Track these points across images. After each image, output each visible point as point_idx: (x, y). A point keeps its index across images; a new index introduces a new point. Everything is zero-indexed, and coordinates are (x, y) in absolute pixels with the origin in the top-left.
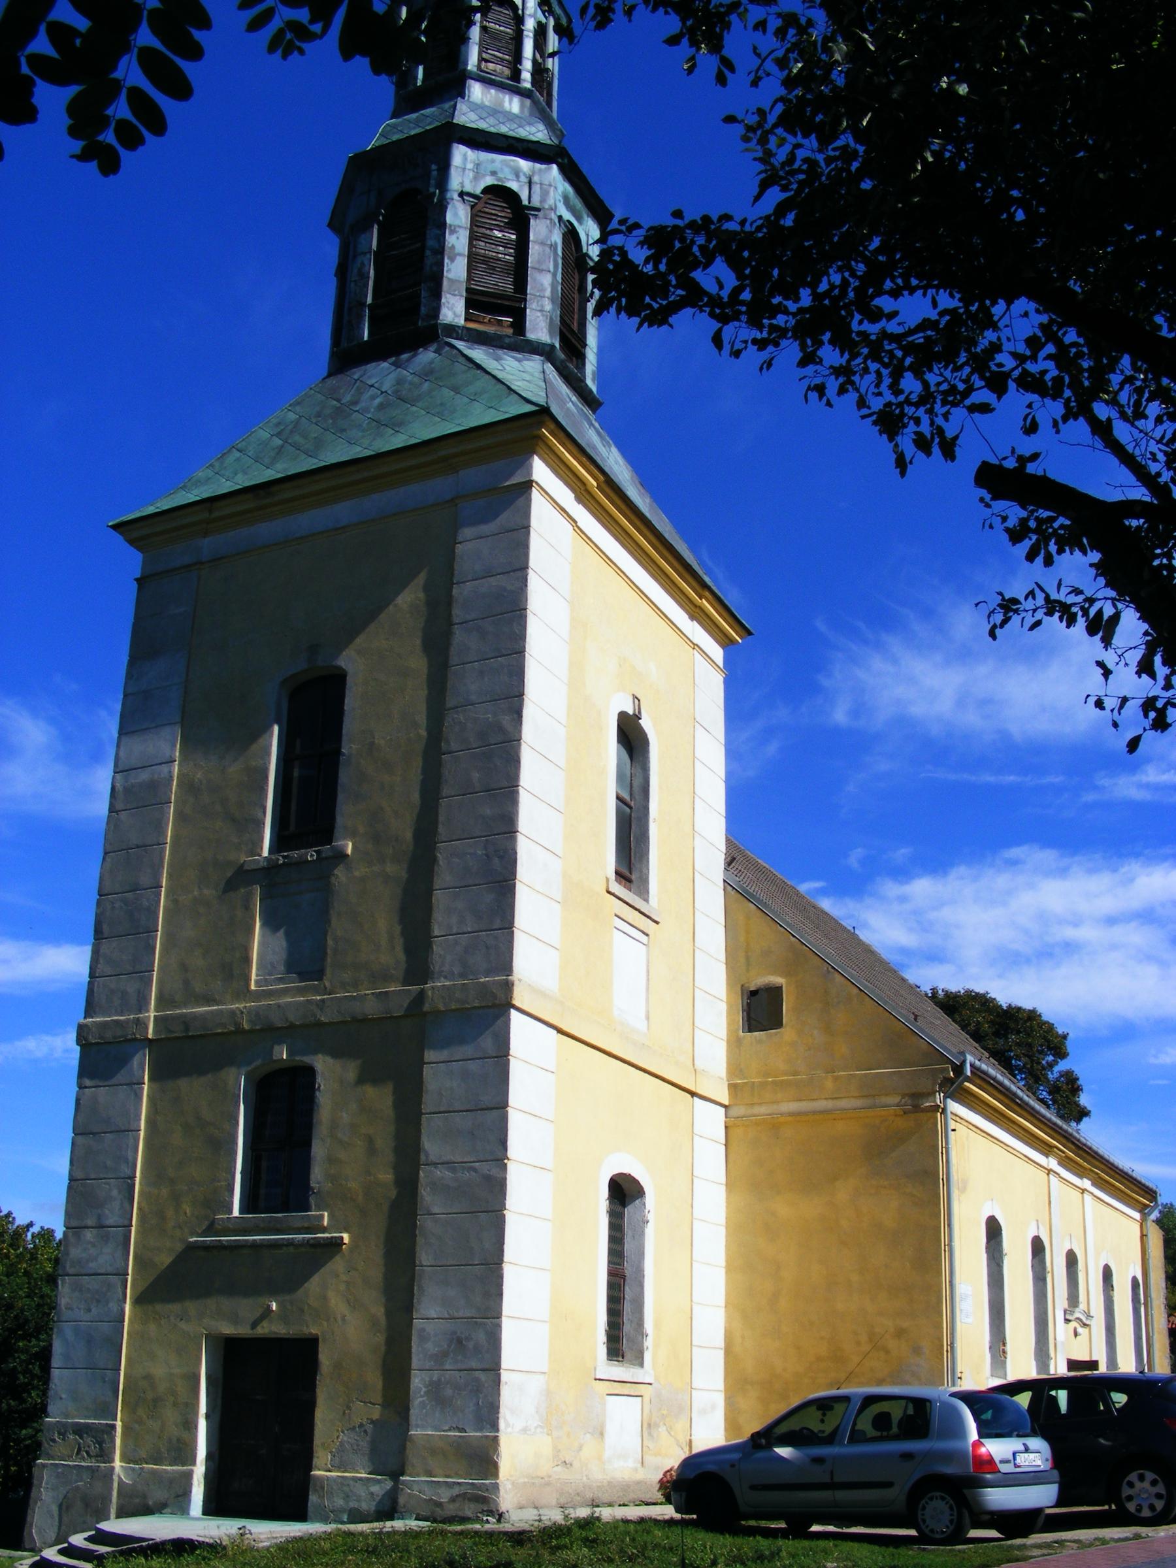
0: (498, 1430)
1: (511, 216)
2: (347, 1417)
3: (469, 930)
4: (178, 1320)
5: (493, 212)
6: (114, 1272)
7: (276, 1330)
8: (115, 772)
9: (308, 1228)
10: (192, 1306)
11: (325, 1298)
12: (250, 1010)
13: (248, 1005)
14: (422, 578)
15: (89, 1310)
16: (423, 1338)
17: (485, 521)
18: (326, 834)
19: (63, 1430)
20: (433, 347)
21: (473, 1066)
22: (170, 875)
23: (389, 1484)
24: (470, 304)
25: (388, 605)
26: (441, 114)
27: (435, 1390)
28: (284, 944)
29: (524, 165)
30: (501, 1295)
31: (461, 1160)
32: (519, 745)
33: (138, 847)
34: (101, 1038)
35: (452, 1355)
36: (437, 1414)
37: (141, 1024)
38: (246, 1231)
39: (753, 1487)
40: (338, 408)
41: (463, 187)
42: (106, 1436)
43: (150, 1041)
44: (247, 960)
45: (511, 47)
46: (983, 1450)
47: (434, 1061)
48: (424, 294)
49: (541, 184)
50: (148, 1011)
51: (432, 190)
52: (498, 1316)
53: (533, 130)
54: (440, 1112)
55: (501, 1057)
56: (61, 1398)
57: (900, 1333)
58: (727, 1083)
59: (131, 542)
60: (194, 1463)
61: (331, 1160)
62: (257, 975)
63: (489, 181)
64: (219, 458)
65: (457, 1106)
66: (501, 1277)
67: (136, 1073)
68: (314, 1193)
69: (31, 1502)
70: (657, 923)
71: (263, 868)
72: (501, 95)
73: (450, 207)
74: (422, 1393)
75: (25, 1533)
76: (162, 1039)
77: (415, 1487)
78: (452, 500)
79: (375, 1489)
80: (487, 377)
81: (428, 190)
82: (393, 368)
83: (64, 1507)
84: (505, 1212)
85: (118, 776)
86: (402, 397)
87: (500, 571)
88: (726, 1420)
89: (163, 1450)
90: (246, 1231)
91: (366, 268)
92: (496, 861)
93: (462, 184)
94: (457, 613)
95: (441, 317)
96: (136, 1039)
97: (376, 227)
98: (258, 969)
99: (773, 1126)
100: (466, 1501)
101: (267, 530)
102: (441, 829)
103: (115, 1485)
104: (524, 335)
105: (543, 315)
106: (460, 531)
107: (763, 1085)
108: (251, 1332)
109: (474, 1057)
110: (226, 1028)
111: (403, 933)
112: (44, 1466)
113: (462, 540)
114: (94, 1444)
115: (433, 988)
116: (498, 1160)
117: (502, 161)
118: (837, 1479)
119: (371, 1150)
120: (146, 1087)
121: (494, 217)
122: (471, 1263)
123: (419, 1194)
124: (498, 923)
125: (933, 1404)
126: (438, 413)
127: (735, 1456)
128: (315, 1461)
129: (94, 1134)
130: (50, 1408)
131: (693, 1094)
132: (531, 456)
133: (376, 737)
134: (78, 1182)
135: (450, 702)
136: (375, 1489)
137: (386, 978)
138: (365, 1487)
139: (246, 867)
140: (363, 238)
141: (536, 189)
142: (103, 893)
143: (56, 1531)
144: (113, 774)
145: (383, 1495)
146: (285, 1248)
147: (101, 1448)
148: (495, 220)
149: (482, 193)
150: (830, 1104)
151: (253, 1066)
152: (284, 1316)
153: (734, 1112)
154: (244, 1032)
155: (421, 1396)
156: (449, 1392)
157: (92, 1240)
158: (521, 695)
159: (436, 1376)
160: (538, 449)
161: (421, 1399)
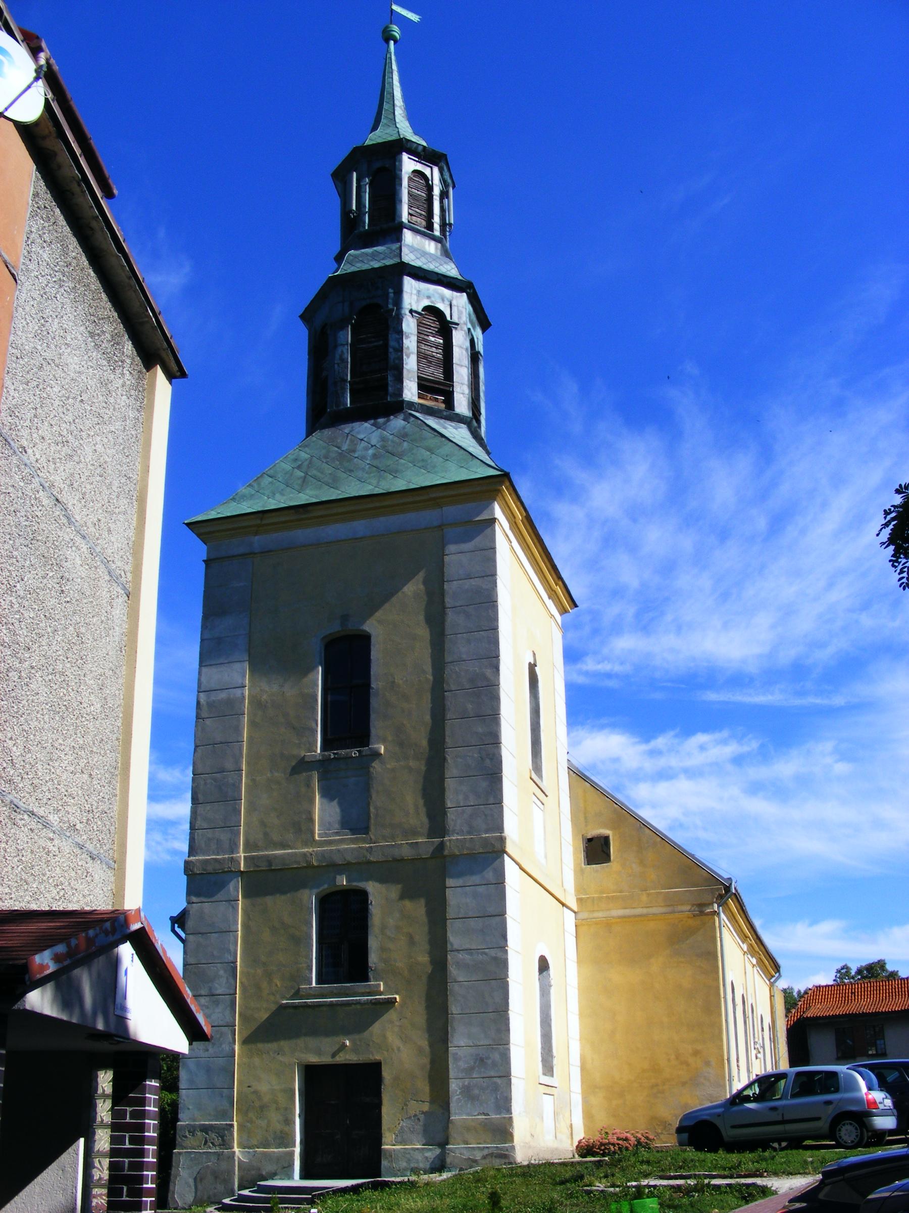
0: (511, 1114)
1: (438, 326)
2: (405, 1111)
3: (472, 804)
4: (276, 1054)
5: (428, 323)
6: (225, 1024)
7: (350, 1058)
8: (199, 692)
9: (369, 993)
10: (284, 1044)
11: (384, 1036)
12: (317, 853)
13: (315, 849)
14: (421, 575)
15: (207, 1050)
16: (457, 1059)
17: (464, 541)
18: (362, 737)
19: (192, 1130)
20: (402, 416)
21: (481, 889)
22: (248, 763)
23: (438, 1151)
24: (421, 387)
25: (397, 592)
26: (390, 253)
27: (467, 1091)
28: (338, 810)
29: (447, 293)
30: (508, 1030)
31: (475, 948)
32: (499, 689)
33: (221, 743)
34: (205, 870)
35: (477, 1069)
36: (469, 1105)
37: (236, 861)
38: (323, 996)
39: (733, 1127)
40: (340, 454)
41: (411, 306)
42: (226, 1132)
43: (242, 872)
44: (311, 820)
45: (425, 206)
46: (870, 1097)
47: (453, 886)
48: (390, 378)
49: (458, 306)
50: (239, 853)
51: (390, 306)
52: (507, 1043)
53: (449, 267)
54: (459, 918)
55: (499, 884)
56: (189, 1109)
57: (696, 1053)
58: (575, 898)
59: (199, 535)
60: (295, 1146)
61: (383, 949)
62: (319, 830)
63: (426, 303)
64: (255, 480)
65: (471, 914)
66: (508, 1019)
67: (232, 893)
68: (372, 970)
69: (172, 1178)
70: (547, 796)
71: (320, 760)
72: (423, 240)
73: (404, 320)
74: (458, 1093)
75: (169, 1199)
76: (251, 871)
77: (457, 1151)
78: (440, 526)
79: (428, 1154)
80: (450, 443)
81: (388, 307)
82: (374, 428)
83: (198, 1179)
84: (508, 979)
85: (201, 695)
86: (387, 451)
87: (476, 576)
88: (583, 1112)
89: (269, 1139)
90: (323, 996)
91: (346, 355)
92: (488, 762)
93: (410, 304)
94: (449, 601)
95: (404, 396)
96: (231, 871)
97: (350, 326)
98: (319, 826)
99: (608, 925)
100: (494, 1158)
101: (302, 534)
102: (448, 740)
103: (237, 1163)
104: (454, 411)
105: (464, 397)
106: (446, 547)
107: (600, 899)
108: (331, 1060)
109: (481, 883)
110: (300, 864)
111: (425, 804)
112: (180, 1153)
113: (448, 553)
114: (217, 1137)
115: (450, 840)
116: (501, 947)
117: (435, 290)
118: (786, 1118)
119: (411, 941)
120: (240, 902)
121: (429, 327)
122: (486, 1011)
123: (448, 969)
124: (491, 800)
125: (839, 1075)
126: (423, 466)
127: (720, 1110)
128: (384, 1140)
129: (202, 934)
130: (180, 1116)
131: (563, 905)
132: (493, 502)
133: (396, 678)
134: (191, 966)
135: (448, 658)
136: (428, 1154)
137: (415, 833)
138: (421, 1154)
139: (307, 759)
140: (341, 334)
141: (455, 309)
142: (196, 773)
143: (194, 1195)
144: (197, 693)
145: (434, 1158)
146: (353, 1006)
147: (223, 1140)
148: (430, 329)
149: (422, 310)
150: (645, 911)
151: (321, 889)
152: (355, 1049)
153: (581, 916)
154: (314, 867)
155: (458, 1095)
156: (476, 1092)
157: (206, 1004)
158: (497, 657)
159: (467, 1082)
160: (498, 499)
161: (457, 1097)
